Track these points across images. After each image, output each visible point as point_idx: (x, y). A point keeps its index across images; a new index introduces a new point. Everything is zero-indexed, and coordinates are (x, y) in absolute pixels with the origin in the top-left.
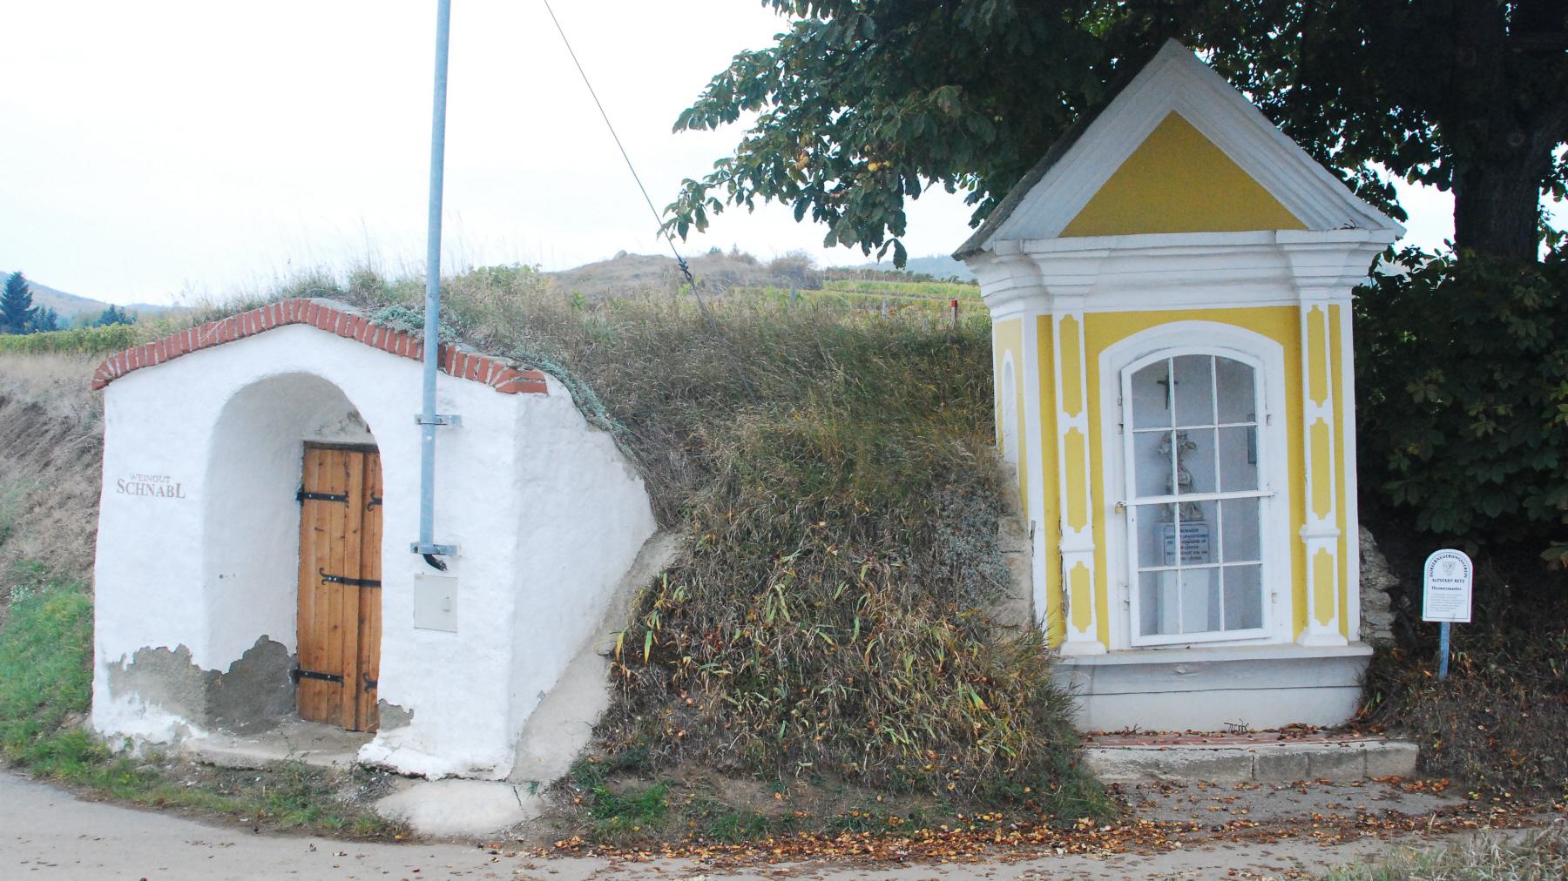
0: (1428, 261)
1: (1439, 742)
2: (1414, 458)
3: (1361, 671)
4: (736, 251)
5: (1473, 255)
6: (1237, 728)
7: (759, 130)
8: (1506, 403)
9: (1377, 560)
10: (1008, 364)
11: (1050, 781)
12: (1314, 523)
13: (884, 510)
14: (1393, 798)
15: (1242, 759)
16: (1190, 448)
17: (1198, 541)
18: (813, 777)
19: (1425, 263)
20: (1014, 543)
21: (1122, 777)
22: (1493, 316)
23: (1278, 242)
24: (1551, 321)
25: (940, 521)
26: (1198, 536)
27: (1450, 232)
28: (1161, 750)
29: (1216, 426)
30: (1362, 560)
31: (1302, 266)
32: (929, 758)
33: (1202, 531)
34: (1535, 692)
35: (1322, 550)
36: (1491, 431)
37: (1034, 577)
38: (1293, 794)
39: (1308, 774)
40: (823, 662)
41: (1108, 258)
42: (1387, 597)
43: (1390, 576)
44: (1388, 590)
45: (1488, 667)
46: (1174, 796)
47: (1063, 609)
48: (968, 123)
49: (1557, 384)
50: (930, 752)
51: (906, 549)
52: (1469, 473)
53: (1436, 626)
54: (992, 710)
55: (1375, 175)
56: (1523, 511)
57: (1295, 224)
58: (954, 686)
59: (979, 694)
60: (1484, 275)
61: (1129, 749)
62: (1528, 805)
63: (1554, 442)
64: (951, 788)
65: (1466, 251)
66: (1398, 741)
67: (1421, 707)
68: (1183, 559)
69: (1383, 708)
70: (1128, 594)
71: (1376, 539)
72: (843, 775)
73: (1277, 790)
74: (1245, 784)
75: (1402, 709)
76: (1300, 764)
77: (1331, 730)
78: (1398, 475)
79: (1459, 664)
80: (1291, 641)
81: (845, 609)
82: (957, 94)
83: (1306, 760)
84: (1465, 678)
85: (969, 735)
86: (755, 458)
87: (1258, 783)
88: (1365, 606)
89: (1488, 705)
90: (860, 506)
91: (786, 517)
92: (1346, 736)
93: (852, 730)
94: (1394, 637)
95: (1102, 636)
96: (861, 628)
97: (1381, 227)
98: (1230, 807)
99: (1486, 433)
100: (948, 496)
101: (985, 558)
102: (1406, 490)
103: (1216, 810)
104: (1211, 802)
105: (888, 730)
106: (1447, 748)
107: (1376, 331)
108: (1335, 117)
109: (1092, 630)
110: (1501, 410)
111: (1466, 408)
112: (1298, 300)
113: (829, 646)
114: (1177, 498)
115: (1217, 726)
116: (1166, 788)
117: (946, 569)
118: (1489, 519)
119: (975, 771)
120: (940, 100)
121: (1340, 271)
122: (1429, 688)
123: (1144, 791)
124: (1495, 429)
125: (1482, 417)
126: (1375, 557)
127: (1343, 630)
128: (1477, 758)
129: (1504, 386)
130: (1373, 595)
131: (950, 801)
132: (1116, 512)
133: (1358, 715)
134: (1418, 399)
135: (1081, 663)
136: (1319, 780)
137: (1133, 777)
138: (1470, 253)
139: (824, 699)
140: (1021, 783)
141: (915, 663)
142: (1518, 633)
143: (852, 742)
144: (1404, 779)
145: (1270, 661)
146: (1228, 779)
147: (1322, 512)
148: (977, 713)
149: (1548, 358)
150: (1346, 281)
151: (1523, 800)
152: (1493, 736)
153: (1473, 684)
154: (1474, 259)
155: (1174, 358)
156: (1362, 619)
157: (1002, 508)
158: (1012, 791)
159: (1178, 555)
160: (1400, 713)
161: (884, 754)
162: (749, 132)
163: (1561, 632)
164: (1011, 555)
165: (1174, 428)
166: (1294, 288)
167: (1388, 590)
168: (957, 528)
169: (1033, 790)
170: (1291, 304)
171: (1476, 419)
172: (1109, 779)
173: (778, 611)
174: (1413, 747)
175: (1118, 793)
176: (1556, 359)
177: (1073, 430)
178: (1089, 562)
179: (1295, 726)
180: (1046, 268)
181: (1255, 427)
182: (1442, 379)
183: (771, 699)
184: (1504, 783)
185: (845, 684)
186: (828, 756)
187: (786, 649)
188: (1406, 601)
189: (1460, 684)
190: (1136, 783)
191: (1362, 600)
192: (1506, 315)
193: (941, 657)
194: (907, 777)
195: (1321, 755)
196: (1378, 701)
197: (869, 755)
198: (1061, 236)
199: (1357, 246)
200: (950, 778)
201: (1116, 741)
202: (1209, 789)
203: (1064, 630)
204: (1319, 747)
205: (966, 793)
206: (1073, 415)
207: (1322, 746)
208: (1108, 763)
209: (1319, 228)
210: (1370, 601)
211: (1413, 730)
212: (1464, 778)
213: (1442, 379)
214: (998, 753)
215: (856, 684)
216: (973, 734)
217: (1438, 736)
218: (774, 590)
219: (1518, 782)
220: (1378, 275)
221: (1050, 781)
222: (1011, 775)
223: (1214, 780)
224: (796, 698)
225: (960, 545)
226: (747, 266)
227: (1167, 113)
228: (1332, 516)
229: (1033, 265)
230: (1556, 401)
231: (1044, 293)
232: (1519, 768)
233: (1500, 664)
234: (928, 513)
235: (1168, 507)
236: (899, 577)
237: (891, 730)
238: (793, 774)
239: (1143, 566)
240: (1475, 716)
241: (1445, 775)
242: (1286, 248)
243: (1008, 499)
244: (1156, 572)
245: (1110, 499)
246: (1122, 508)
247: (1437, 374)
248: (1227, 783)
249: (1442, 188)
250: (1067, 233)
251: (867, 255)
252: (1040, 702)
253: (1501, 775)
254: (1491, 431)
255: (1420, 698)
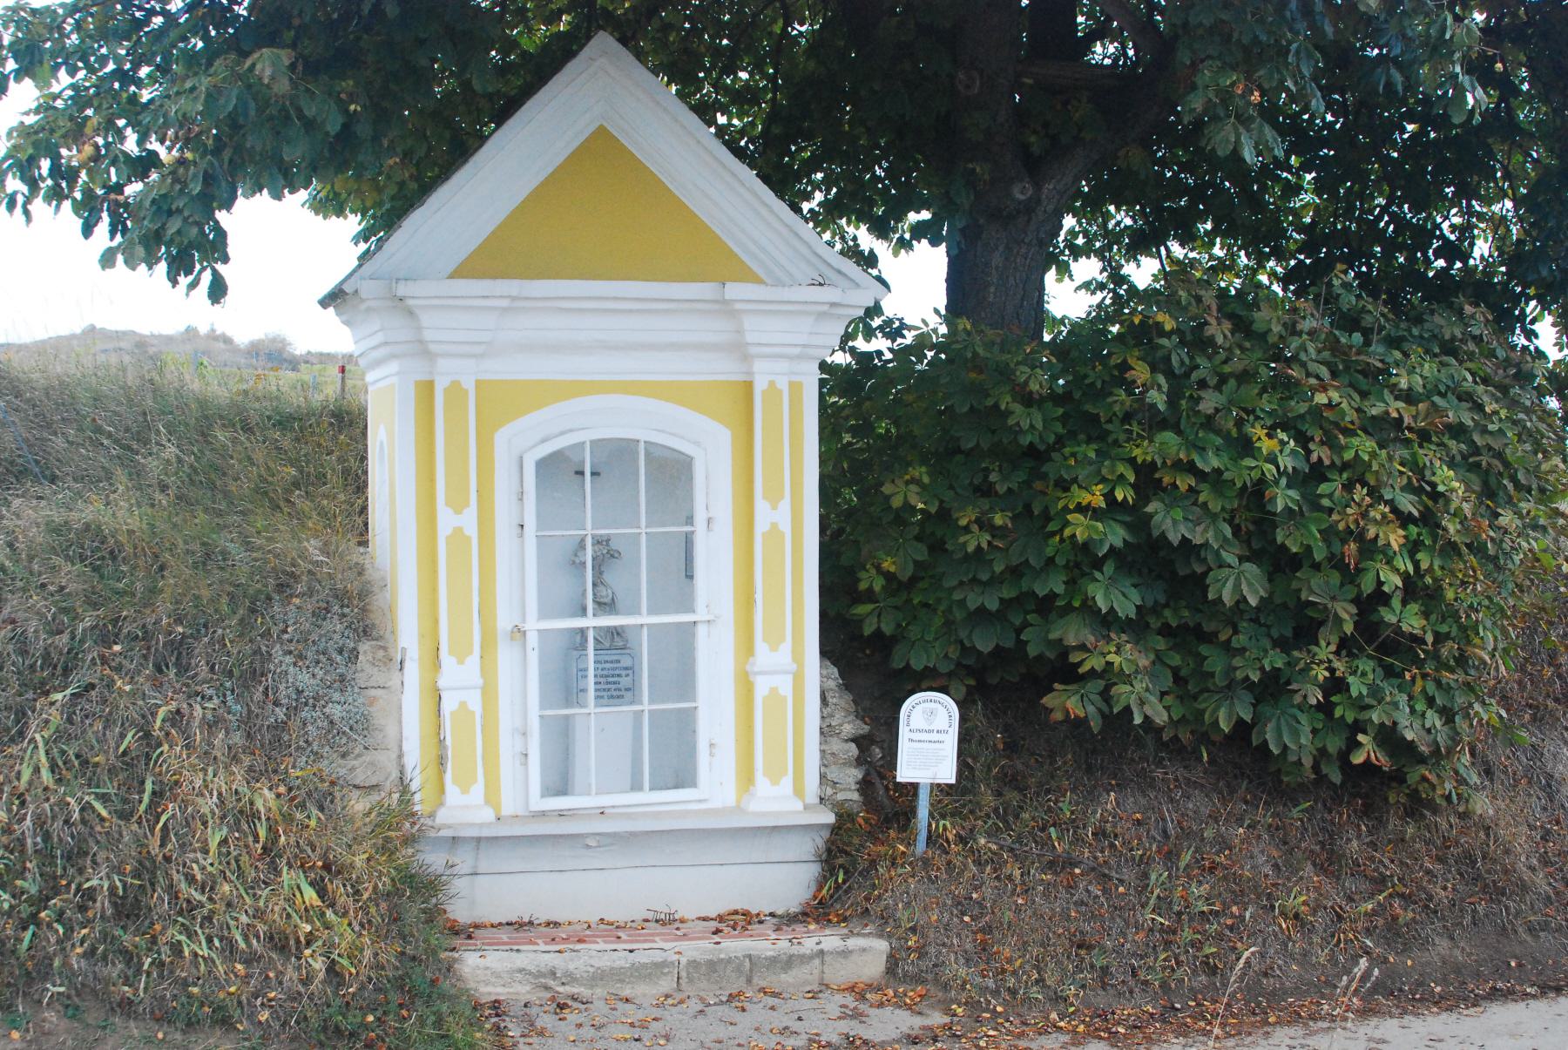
0: (914, 333)
1: (914, 938)
2: (889, 576)
3: (820, 843)
4: (213, 330)
5: (969, 327)
6: (663, 916)
7: (37, 111)
8: (1002, 511)
9: (843, 703)
10: (382, 443)
11: (401, 1006)
12: (764, 656)
13: (203, 631)
14: (857, 1015)
15: (664, 964)
16: (612, 556)
17: (619, 676)
18: (70, 1007)
19: (909, 338)
20: (378, 677)
21: (507, 990)
22: (990, 402)
23: (727, 297)
24: (1060, 411)
25: (278, 646)
26: (620, 669)
27: (941, 302)
28: (559, 952)
29: (643, 531)
30: (824, 701)
31: (759, 330)
32: (236, 976)
33: (626, 662)
34: (1032, 871)
35: (774, 691)
36: (985, 545)
37: (404, 720)
38: (726, 1012)
39: (749, 981)
40: (92, 844)
41: (505, 310)
42: (853, 749)
43: (858, 722)
44: (855, 740)
45: (975, 840)
46: (572, 1018)
47: (441, 761)
48: (302, 103)
49: (1067, 489)
50: (239, 966)
51: (228, 684)
52: (957, 596)
53: (914, 787)
54: (328, 907)
55: (855, 239)
56: (1022, 645)
57: (747, 276)
58: (278, 873)
59: (312, 884)
60: (980, 351)
61: (518, 951)
62: (1024, 1023)
63: (1060, 561)
64: (263, 1019)
65: (959, 321)
66: (864, 935)
67: (892, 890)
68: (597, 697)
69: (846, 892)
70: (526, 744)
71: (841, 674)
72: (110, 1003)
73: (709, 1005)
74: (667, 996)
75: (870, 894)
76: (739, 969)
77: (781, 917)
78: (869, 596)
79: (939, 836)
80: (734, 804)
81: (131, 767)
82: (287, 63)
83: (747, 963)
84: (947, 853)
85: (292, 942)
86: (31, 558)
87: (684, 996)
88: (826, 758)
89: (976, 889)
90: (169, 624)
91: (65, 638)
92: (799, 928)
93: (128, 939)
94: (861, 799)
95: (492, 797)
96: (154, 793)
97: (857, 285)
98: (646, 1036)
99: (979, 548)
100: (294, 614)
101: (336, 696)
102: (879, 616)
103: (626, 1040)
104: (620, 1026)
105: (180, 937)
106: (924, 946)
107: (847, 418)
108: (812, 165)
109: (478, 791)
110: (998, 520)
111: (955, 515)
112: (750, 373)
113: (103, 820)
114: (590, 622)
115: (640, 915)
116: (562, 1007)
117: (280, 713)
118: (980, 653)
119: (299, 993)
120: (259, 67)
121: (803, 339)
122: (903, 866)
123: (533, 1011)
124: (989, 543)
125: (975, 528)
126: (841, 697)
127: (798, 791)
128: (962, 961)
129: (1001, 489)
130: (836, 745)
131: (262, 1037)
132: (512, 639)
133: (815, 897)
134: (897, 502)
135: (462, 834)
136: (763, 991)
137: (520, 991)
138: (964, 324)
139: (91, 894)
140: (361, 1008)
141: (224, 842)
142: (1013, 797)
143: (129, 957)
144: (870, 987)
145: (705, 831)
146: (647, 992)
147: (774, 642)
148: (306, 910)
149: (1055, 456)
150: (811, 351)
151: (1019, 1015)
152: (982, 930)
153: (958, 861)
154: (969, 333)
155: (591, 442)
156: (823, 777)
157: (366, 631)
158: (347, 1024)
159: (591, 693)
160: (867, 899)
161: (172, 972)
162: (27, 113)
163: (1064, 796)
164: (373, 692)
165: (589, 531)
166: (746, 358)
167: (855, 740)
168: (301, 657)
169: (378, 1019)
170: (742, 378)
171: (967, 529)
172: (490, 994)
173: (37, 770)
174: (882, 946)
175: (497, 1015)
176: (1066, 459)
177: (458, 531)
178: (475, 704)
179: (736, 912)
180: (426, 319)
181: (693, 532)
182: (926, 479)
183: (14, 896)
184: (996, 993)
185: (121, 873)
186: (91, 976)
187: (40, 822)
188: (877, 752)
189: (940, 861)
190: (524, 999)
191: (823, 752)
192: (1006, 402)
193: (262, 833)
194: (202, 1005)
195: (766, 958)
196: (840, 881)
197: (149, 974)
198: (451, 277)
199: (826, 308)
200: (262, 1004)
201: (505, 938)
202: (620, 1005)
203: (441, 790)
204: (763, 944)
205: (284, 1024)
206: (458, 511)
207: (767, 944)
208: (489, 972)
209: (779, 283)
210: (833, 754)
211: (885, 922)
212: (946, 987)
213: (926, 479)
214: (332, 969)
215: (137, 874)
216: (298, 941)
217: (913, 930)
218: (33, 740)
219: (1013, 992)
220: (853, 351)
221: (401, 1006)
222: (348, 998)
223: (627, 992)
224: (51, 894)
225: (304, 679)
226: (222, 345)
227: (592, 129)
228: (786, 648)
229: (410, 313)
230: (1066, 510)
231: (423, 351)
232: (1014, 973)
233: (989, 834)
234: (262, 636)
235: (582, 632)
236: (211, 725)
237: (183, 938)
238: (40, 1002)
239: (551, 708)
240: (959, 903)
241: (924, 982)
242: (738, 306)
243: (375, 617)
244: (567, 717)
245: (504, 621)
246: (519, 633)
247: (920, 472)
248: (645, 995)
249: (934, 243)
250: (457, 274)
251: (174, 287)
252: (398, 893)
253: (991, 983)
254: (985, 545)
255: (891, 879)
